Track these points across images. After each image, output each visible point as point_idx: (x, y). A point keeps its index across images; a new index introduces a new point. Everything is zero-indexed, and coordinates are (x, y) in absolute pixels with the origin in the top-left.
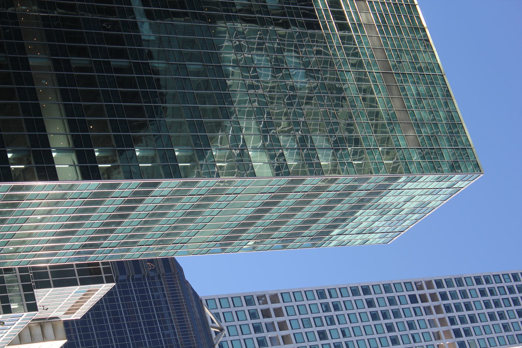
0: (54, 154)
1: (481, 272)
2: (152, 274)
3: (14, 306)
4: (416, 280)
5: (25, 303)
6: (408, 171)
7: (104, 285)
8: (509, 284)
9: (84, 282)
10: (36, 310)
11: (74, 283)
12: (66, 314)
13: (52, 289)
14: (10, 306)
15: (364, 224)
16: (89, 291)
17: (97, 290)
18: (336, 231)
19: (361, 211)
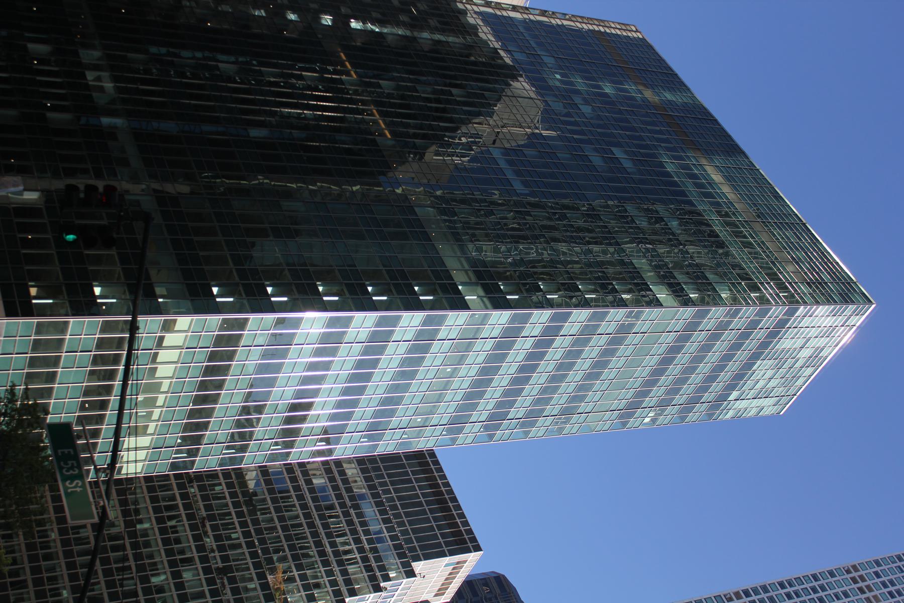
0: (460, 287)
1: (784, 578)
2: (488, 596)
3: (392, 574)
4: (725, 593)
5: (402, 570)
6: (805, 303)
7: (472, 554)
8: (811, 585)
9: (452, 553)
10: (415, 576)
11: (442, 555)
12: (436, 595)
13: (422, 562)
14: (388, 575)
15: (758, 386)
16: (458, 563)
17: (465, 562)
18: (734, 394)
19: (759, 362)
